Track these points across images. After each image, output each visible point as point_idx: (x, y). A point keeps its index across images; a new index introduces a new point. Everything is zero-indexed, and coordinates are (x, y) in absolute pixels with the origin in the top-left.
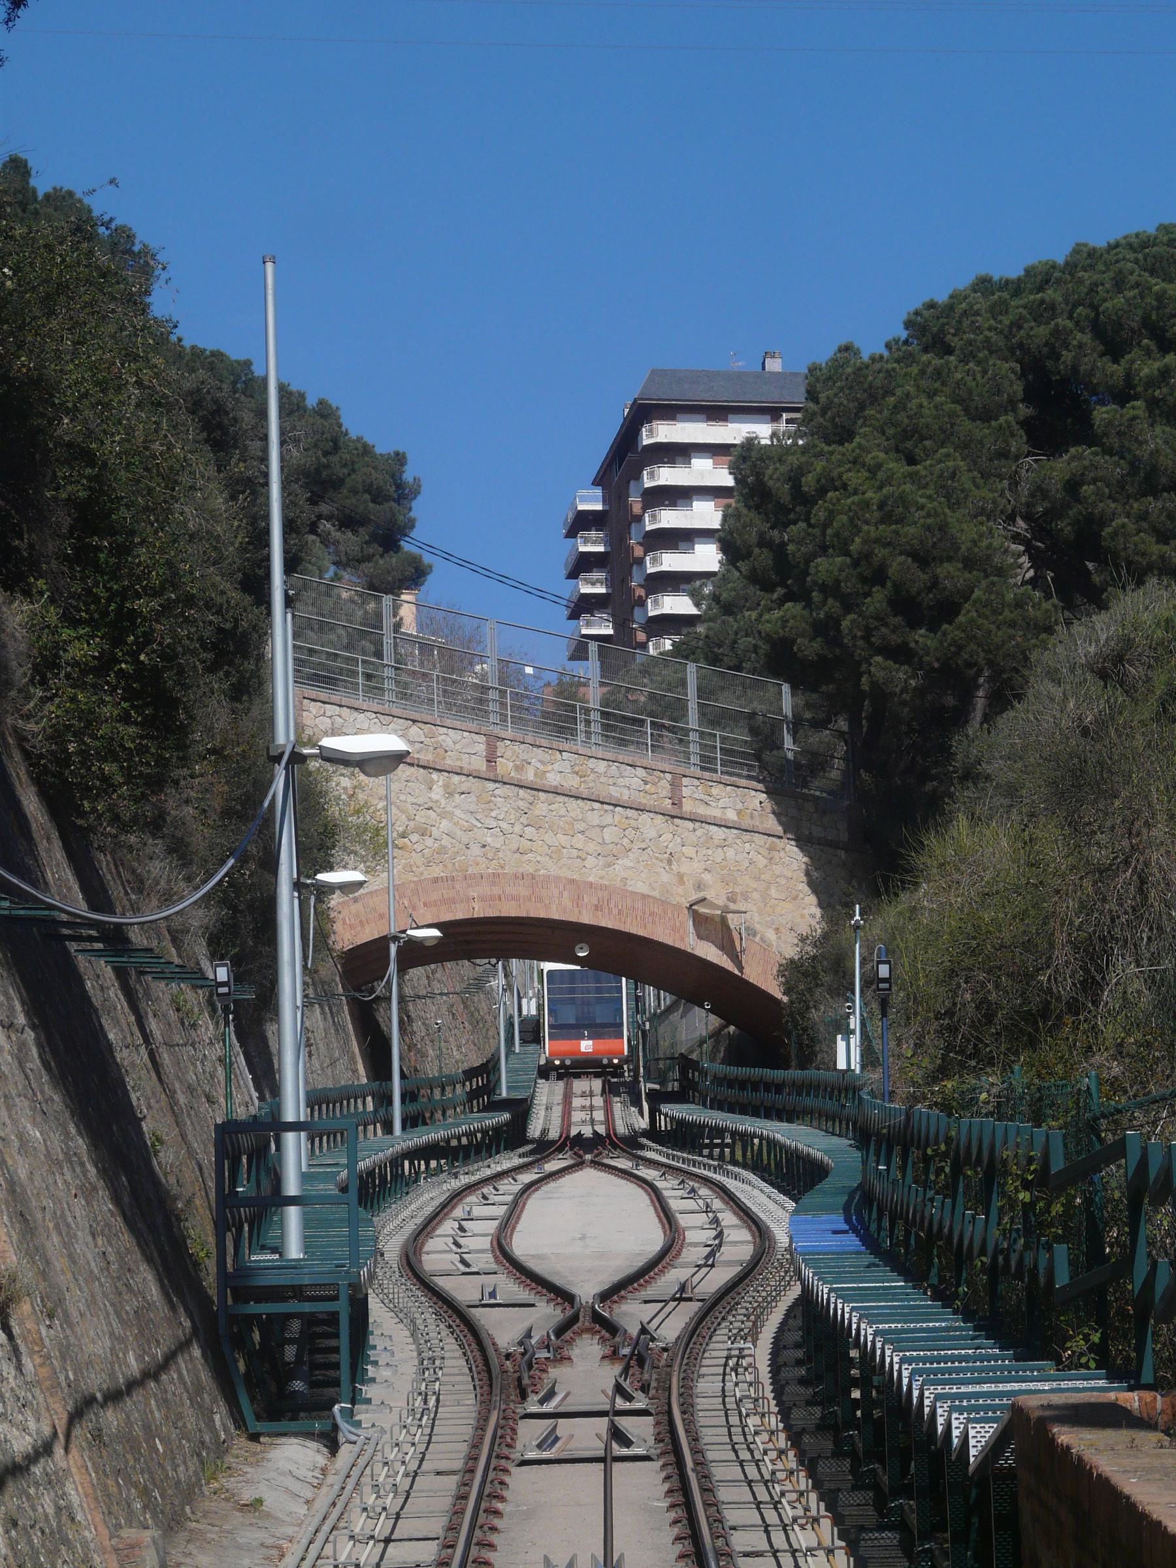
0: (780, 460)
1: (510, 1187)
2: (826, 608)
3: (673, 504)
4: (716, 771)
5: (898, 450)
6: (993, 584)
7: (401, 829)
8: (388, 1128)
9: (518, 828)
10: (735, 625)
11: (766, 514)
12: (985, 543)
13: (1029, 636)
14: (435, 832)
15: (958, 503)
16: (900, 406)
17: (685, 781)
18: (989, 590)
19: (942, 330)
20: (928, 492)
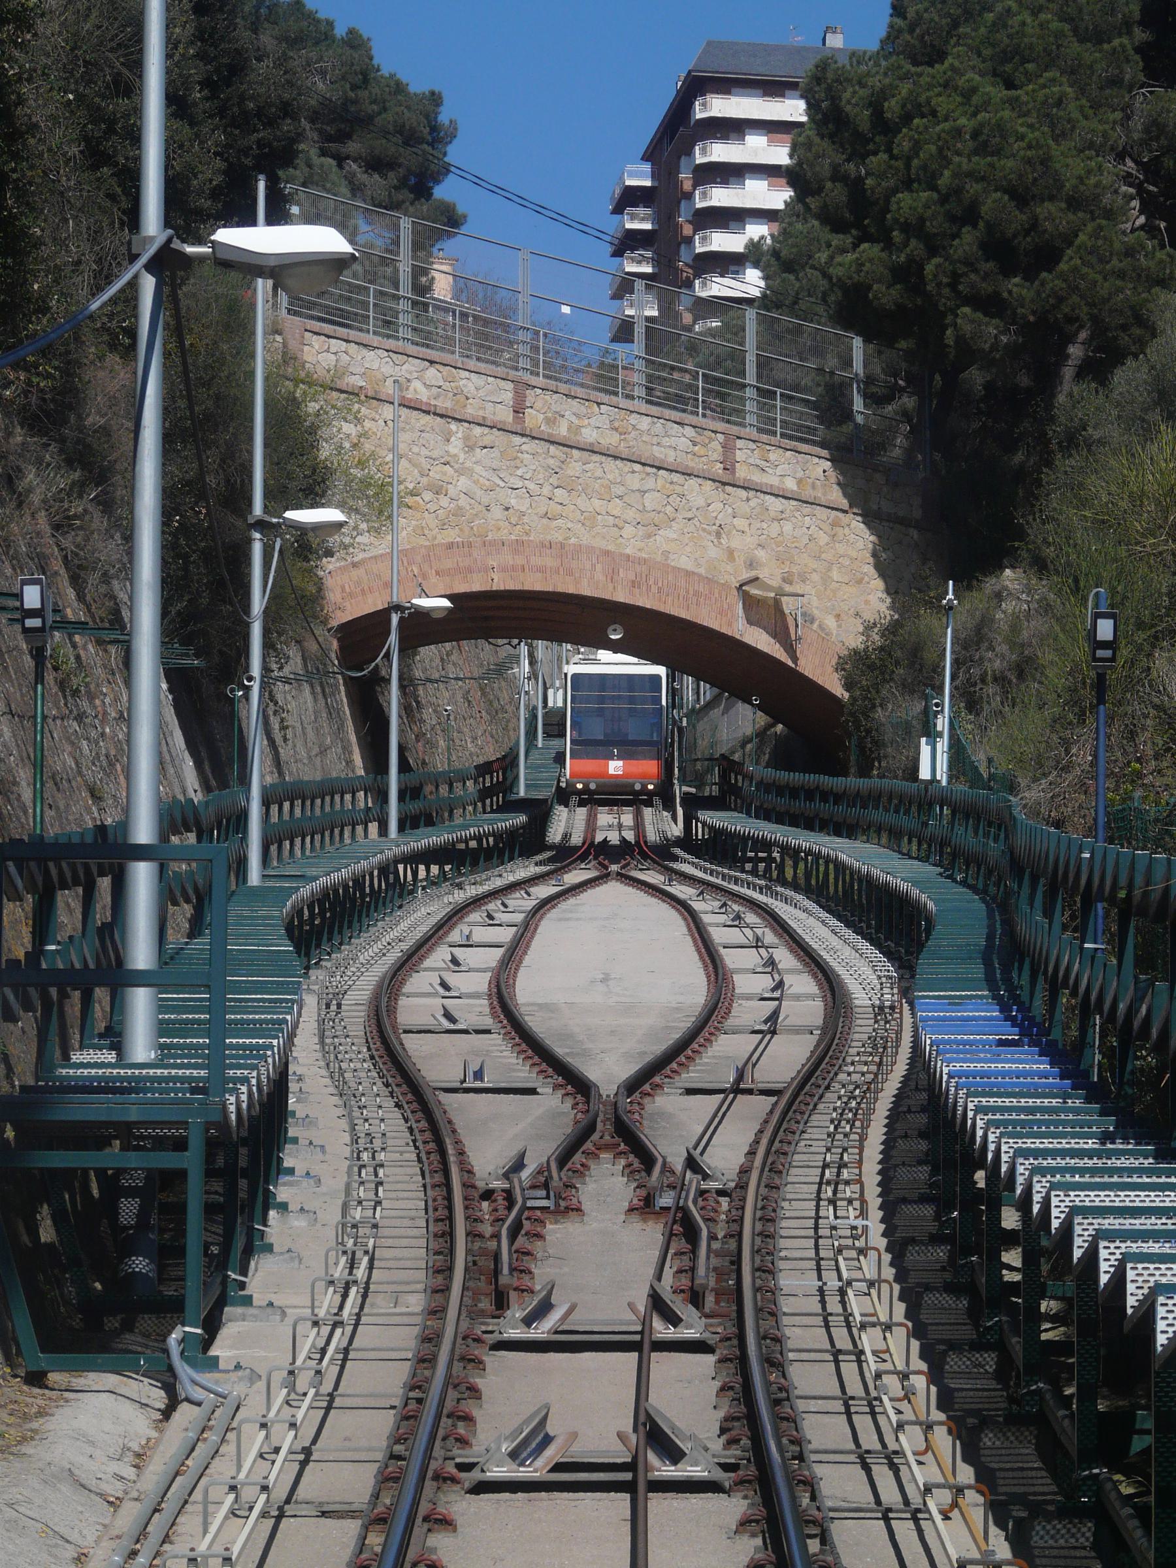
1: (522, 903)
3: (725, 182)
4: (774, 433)
5: (995, 75)
6: (1101, 228)
7: (411, 486)
8: (383, 831)
9: (546, 490)
10: (797, 285)
12: (1092, 180)
14: (452, 491)
15: (1063, 134)
16: (1000, 23)
17: (740, 443)
18: (1095, 235)
20: (1030, 120)
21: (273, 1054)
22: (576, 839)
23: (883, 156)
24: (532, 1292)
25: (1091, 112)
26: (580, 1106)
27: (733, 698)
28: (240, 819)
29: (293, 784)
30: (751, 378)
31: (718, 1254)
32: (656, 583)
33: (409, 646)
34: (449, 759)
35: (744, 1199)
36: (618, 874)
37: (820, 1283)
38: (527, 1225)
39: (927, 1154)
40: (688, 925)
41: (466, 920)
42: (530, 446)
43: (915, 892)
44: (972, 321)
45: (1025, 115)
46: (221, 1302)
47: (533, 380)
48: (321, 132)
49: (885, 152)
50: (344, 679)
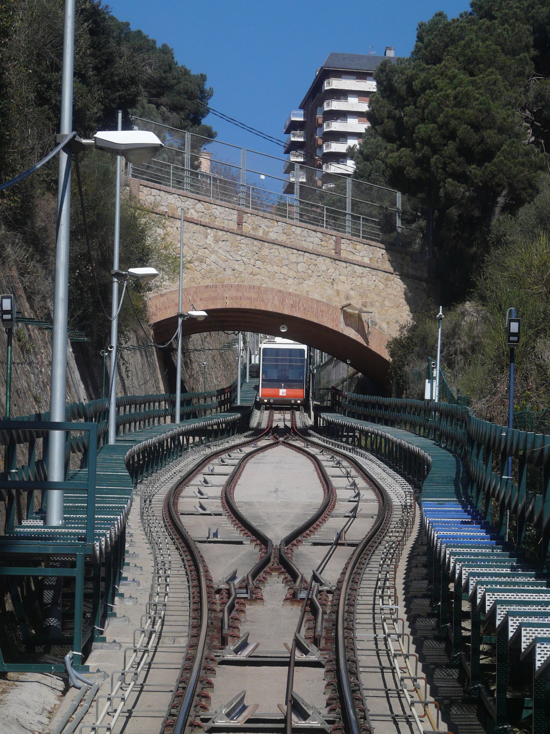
0: (401, 72)
2: (423, 151)
3: (338, 99)
5: (465, 69)
6: (513, 142)
7: (189, 259)
8: (173, 420)
9: (252, 261)
10: (371, 167)
11: (393, 102)
12: (510, 120)
13: (532, 171)
14: (208, 261)
15: (497, 98)
16: (468, 45)
18: (511, 145)
19: (490, 9)
20: (481, 91)
21: (118, 523)
22: (264, 425)
23: (412, 107)
24: (239, 637)
26: (263, 550)
28: (106, 412)
31: (327, 621)
33: (186, 334)
35: (339, 595)
36: (283, 442)
38: (237, 606)
39: (426, 575)
40: (315, 467)
42: (245, 240)
43: (422, 452)
44: (453, 185)
46: (91, 640)
47: (247, 210)
48: (149, 92)
49: (413, 105)
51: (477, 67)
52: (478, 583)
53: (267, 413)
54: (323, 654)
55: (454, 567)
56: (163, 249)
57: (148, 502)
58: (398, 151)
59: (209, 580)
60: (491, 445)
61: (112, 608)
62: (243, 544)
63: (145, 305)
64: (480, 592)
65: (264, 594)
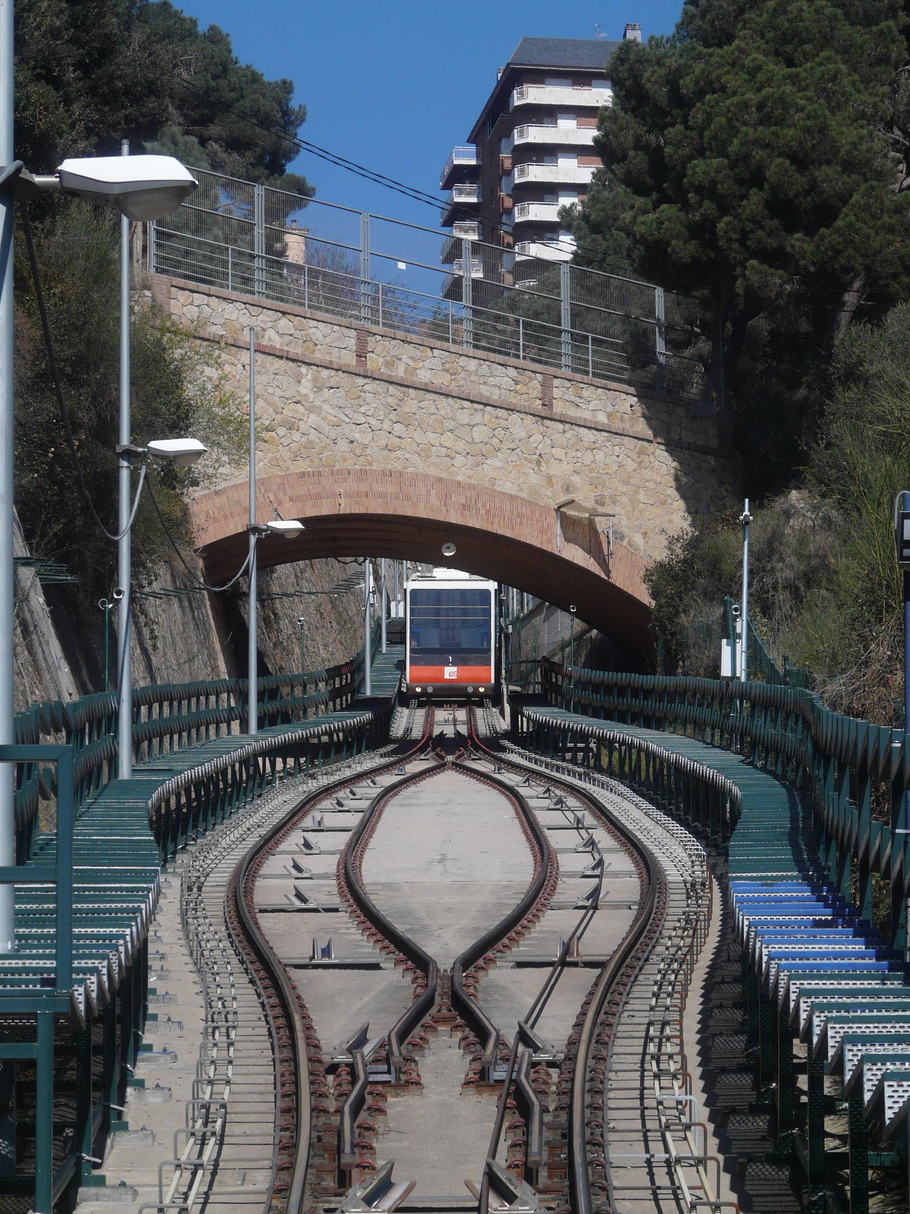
0: (658, 63)
3: (540, 161)
4: (587, 373)
5: (777, 54)
6: (872, 188)
7: (267, 423)
9: (386, 425)
10: (605, 244)
11: (643, 118)
12: (864, 147)
14: (303, 426)
15: (838, 107)
17: (556, 382)
20: (809, 94)
21: (126, 943)
22: (417, 733)
23: (680, 127)
24: (374, 1169)
25: (862, 86)
26: (420, 980)
27: (553, 607)
28: (113, 717)
29: (162, 686)
30: (566, 324)
31: (550, 1127)
32: (484, 506)
33: (266, 565)
34: (303, 664)
35: (573, 1071)
36: (454, 764)
37: (648, 1156)
38: (369, 1100)
39: (742, 1024)
40: (516, 809)
41: (318, 807)
42: (372, 386)
43: (721, 778)
44: (760, 272)
45: (804, 90)
46: (76, 1182)
47: (374, 329)
48: (186, 116)
49: (681, 123)
50: (209, 595)
51: (799, 50)
52: (828, 1020)
53: (421, 713)
54: (545, 1201)
55: (809, 1020)
56: (218, 405)
57: (195, 890)
58: (654, 210)
59: (313, 1045)
60: (869, 765)
61: (120, 1115)
62: (381, 968)
63: (185, 510)
64: (852, 1056)
65: (422, 1072)
